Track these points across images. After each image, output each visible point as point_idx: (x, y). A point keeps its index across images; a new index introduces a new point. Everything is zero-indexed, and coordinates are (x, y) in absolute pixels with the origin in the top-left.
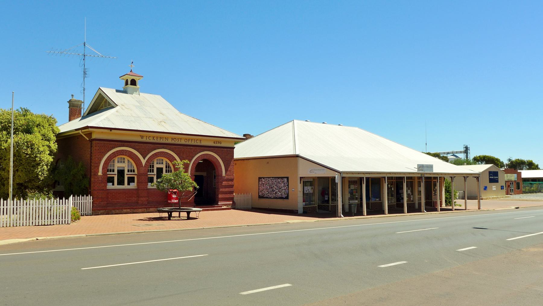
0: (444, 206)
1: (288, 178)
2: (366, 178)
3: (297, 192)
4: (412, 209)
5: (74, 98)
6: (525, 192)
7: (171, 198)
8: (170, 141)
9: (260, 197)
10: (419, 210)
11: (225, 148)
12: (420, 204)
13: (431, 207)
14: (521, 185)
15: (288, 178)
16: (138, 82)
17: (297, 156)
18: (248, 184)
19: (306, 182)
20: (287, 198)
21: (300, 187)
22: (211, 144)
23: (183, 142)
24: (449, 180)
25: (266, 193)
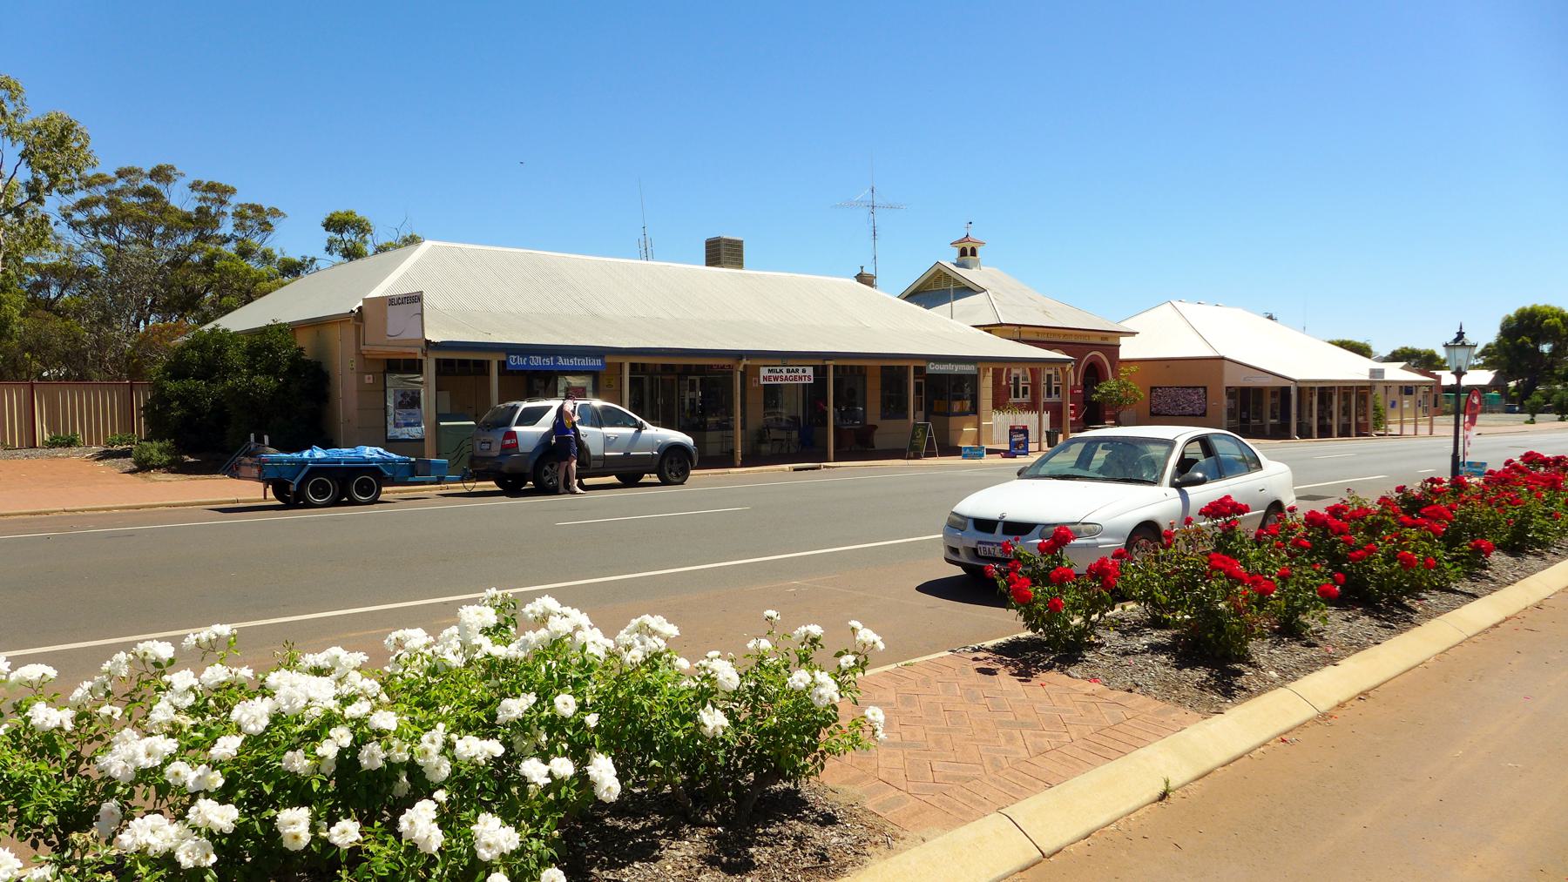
2: (835, 367)
4: (1305, 433)
5: (866, 271)
8: (1061, 339)
11: (1107, 343)
12: (1311, 429)
16: (979, 250)
17: (1223, 358)
19: (1232, 392)
22: (1098, 341)
23: (1073, 340)
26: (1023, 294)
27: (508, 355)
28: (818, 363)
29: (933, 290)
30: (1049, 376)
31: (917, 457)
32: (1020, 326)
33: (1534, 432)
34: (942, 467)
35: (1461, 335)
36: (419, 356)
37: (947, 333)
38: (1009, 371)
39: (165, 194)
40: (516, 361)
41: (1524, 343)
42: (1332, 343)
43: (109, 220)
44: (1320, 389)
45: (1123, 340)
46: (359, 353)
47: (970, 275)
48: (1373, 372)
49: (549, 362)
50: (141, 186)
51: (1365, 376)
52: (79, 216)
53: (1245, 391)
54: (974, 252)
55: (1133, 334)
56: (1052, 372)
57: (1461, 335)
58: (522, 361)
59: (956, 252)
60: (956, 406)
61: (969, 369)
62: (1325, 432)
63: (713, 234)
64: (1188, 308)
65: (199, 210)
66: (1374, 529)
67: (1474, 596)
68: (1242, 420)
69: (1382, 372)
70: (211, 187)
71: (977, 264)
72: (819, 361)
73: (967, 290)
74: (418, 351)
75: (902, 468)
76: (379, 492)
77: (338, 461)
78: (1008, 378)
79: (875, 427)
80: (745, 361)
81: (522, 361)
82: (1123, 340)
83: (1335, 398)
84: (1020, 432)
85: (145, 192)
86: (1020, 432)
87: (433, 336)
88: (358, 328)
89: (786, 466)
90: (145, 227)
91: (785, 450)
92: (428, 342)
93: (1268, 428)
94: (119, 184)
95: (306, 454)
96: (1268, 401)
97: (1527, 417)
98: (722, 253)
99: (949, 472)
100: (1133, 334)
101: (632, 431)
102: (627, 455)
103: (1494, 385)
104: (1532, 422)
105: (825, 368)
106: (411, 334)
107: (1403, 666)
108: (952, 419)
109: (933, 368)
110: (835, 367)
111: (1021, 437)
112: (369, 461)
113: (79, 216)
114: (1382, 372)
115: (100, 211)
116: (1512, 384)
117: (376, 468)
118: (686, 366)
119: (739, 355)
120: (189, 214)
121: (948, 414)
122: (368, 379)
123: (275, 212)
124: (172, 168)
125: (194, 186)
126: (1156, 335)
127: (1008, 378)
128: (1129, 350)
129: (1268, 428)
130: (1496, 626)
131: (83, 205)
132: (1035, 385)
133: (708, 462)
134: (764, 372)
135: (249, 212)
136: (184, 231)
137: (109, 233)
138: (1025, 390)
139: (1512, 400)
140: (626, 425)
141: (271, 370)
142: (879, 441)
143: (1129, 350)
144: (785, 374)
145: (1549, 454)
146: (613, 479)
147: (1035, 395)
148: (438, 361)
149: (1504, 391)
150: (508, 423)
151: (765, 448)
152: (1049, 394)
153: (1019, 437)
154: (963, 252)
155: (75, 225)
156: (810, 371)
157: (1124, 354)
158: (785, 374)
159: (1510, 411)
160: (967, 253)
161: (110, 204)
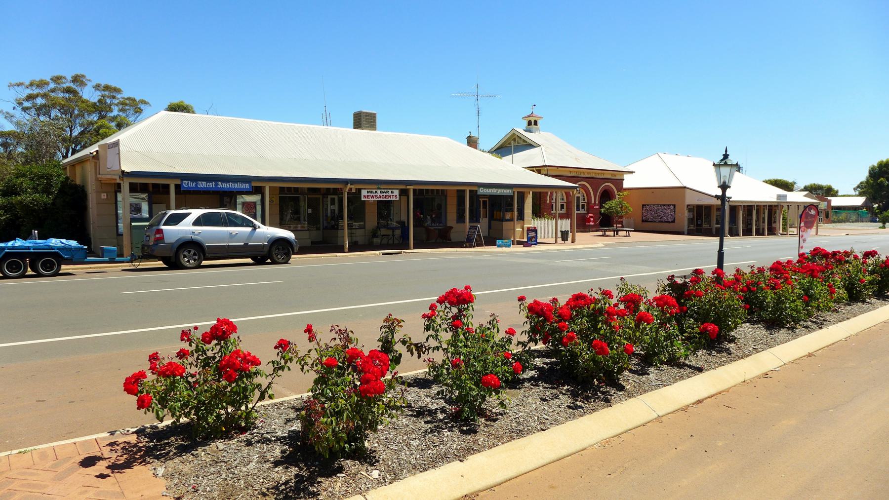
0: (781, 231)
1: (674, 206)
2: (470, 191)
3: (684, 216)
4: (759, 233)
5: (472, 135)
6: (834, 222)
7: (589, 221)
8: (586, 175)
9: (643, 221)
10: (763, 234)
11: (616, 178)
12: (763, 229)
13: (772, 232)
14: (831, 213)
15: (674, 206)
16: (539, 122)
17: (685, 188)
18: (632, 208)
19: (690, 208)
20: (673, 221)
21: (686, 213)
22: (609, 177)
23: (593, 176)
24: (785, 208)
25: (650, 218)
26: (562, 149)
27: (182, 180)
28: (403, 187)
29: (510, 146)
30: (578, 198)
31: (470, 246)
32: (558, 167)
33: (882, 234)
34: (471, 253)
35: (726, 156)
36: (118, 181)
37: (513, 171)
38: (552, 193)
39: (81, 93)
40: (187, 185)
41: (882, 182)
42: (766, 182)
43: (44, 106)
44: (757, 206)
45: (626, 177)
46: (97, 179)
47: (531, 137)
48: (779, 196)
49: (211, 185)
50: (65, 86)
51: (774, 199)
52: (26, 104)
53: (699, 208)
54: (536, 123)
55: (632, 172)
56: (580, 195)
57: (726, 156)
58: (192, 185)
59: (525, 123)
60: (508, 216)
61: (508, 192)
62: (747, 232)
63: (357, 110)
64: (669, 158)
65: (99, 101)
66: (562, 317)
67: (700, 370)
68: (698, 225)
69: (785, 196)
70: (107, 88)
71: (538, 130)
72: (404, 187)
73: (530, 145)
74: (117, 177)
75: (427, 254)
76: (59, 268)
77: (29, 248)
78: (551, 199)
79: (451, 228)
80: (349, 186)
81: (192, 185)
82: (626, 177)
83: (741, 213)
84: (532, 231)
85: (68, 90)
86: (532, 231)
87: (126, 168)
88: (96, 163)
89: (377, 252)
90: (65, 109)
91: (391, 242)
92: (123, 172)
93: (714, 230)
94: (52, 85)
95: (10, 244)
96: (714, 214)
97: (881, 224)
98: (364, 121)
99: (470, 257)
100: (632, 172)
101: (249, 229)
102: (246, 245)
103: (864, 205)
104: (884, 227)
105: (464, 191)
106: (116, 168)
107: (553, 456)
108: (504, 223)
109: (482, 191)
110: (470, 191)
111: (533, 234)
112: (52, 248)
113: (26, 104)
114: (785, 196)
115: (40, 101)
116: (876, 206)
117: (57, 253)
118: (327, 189)
119: (346, 182)
120: (95, 104)
121: (503, 220)
122: (104, 196)
123: (144, 102)
124: (83, 76)
125: (97, 87)
126: (645, 173)
127: (551, 199)
128: (629, 182)
129: (714, 230)
130: (699, 402)
131: (30, 98)
132: (569, 203)
133: (303, 250)
134: (364, 193)
135: (127, 102)
136: (90, 114)
137: (47, 114)
138: (583, 206)
139: (876, 214)
140: (248, 226)
141: (47, 190)
142: (454, 236)
143: (629, 182)
144: (379, 194)
145: (830, 250)
146: (249, 260)
147: (569, 209)
148: (130, 184)
149: (870, 209)
150: (159, 224)
151: (376, 241)
152: (578, 209)
153: (532, 234)
154: (530, 123)
155: (25, 109)
156: (396, 192)
157: (626, 185)
158: (379, 194)
159: (873, 221)
160: (532, 123)
161: (45, 96)
